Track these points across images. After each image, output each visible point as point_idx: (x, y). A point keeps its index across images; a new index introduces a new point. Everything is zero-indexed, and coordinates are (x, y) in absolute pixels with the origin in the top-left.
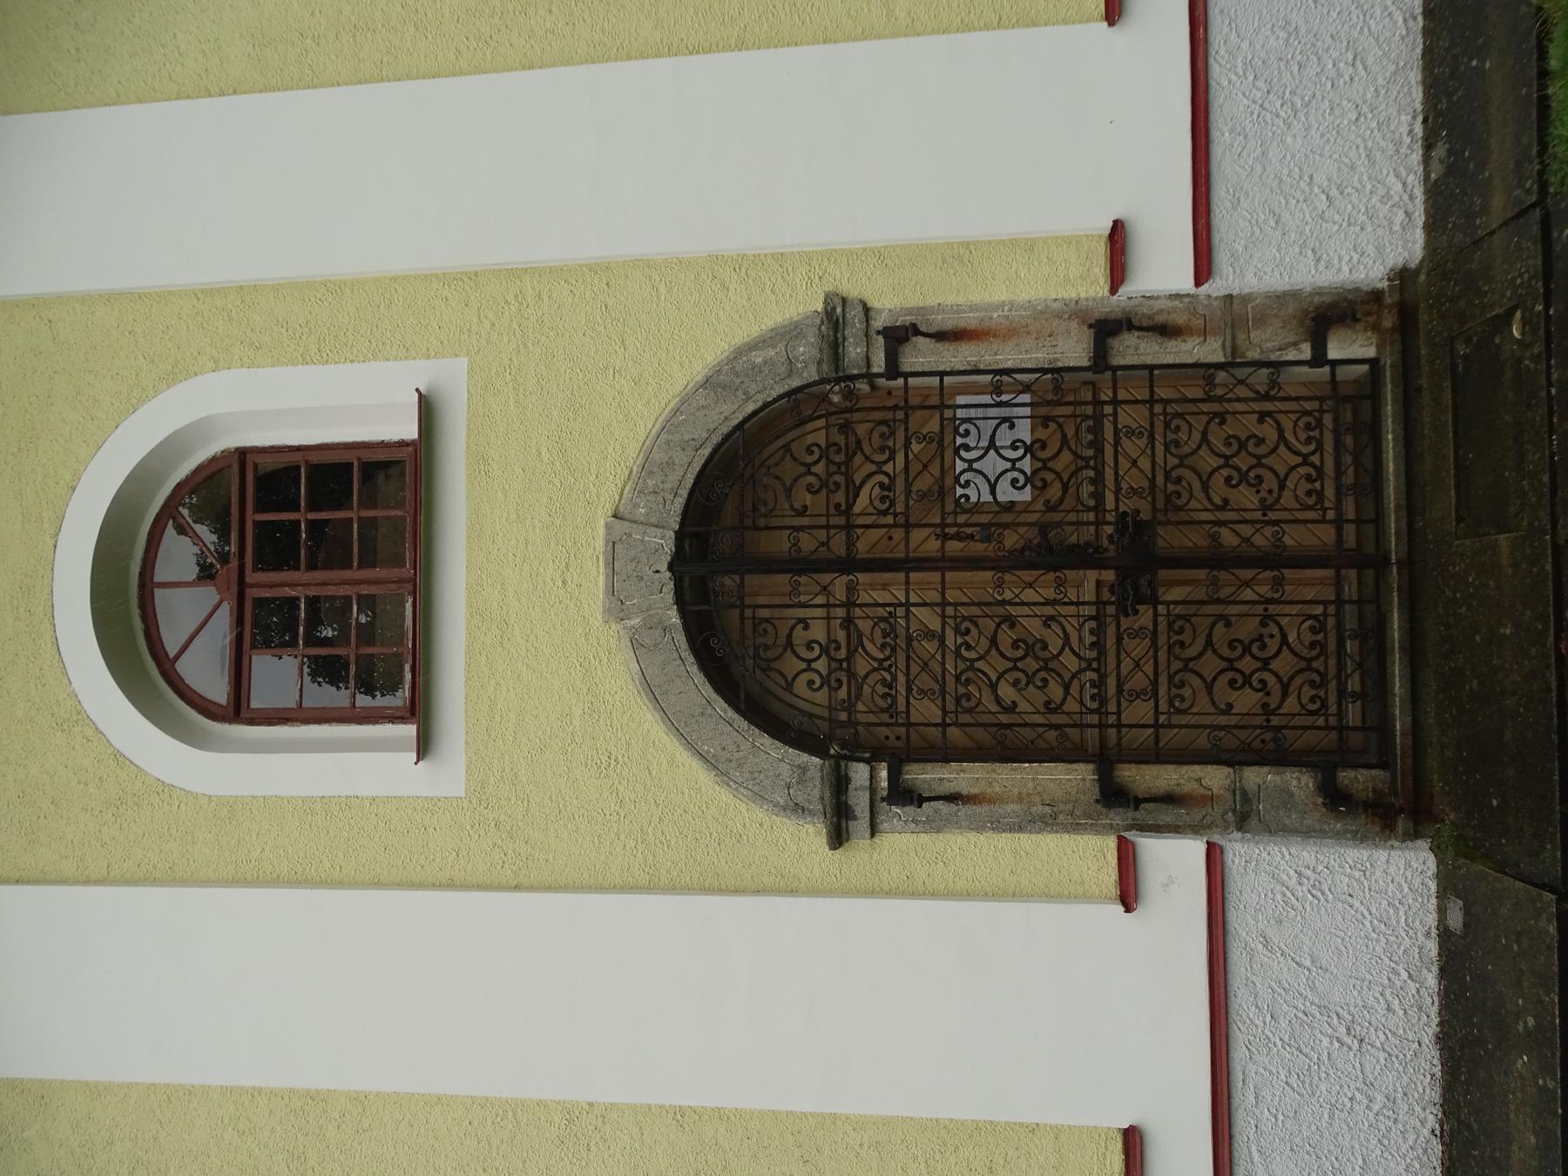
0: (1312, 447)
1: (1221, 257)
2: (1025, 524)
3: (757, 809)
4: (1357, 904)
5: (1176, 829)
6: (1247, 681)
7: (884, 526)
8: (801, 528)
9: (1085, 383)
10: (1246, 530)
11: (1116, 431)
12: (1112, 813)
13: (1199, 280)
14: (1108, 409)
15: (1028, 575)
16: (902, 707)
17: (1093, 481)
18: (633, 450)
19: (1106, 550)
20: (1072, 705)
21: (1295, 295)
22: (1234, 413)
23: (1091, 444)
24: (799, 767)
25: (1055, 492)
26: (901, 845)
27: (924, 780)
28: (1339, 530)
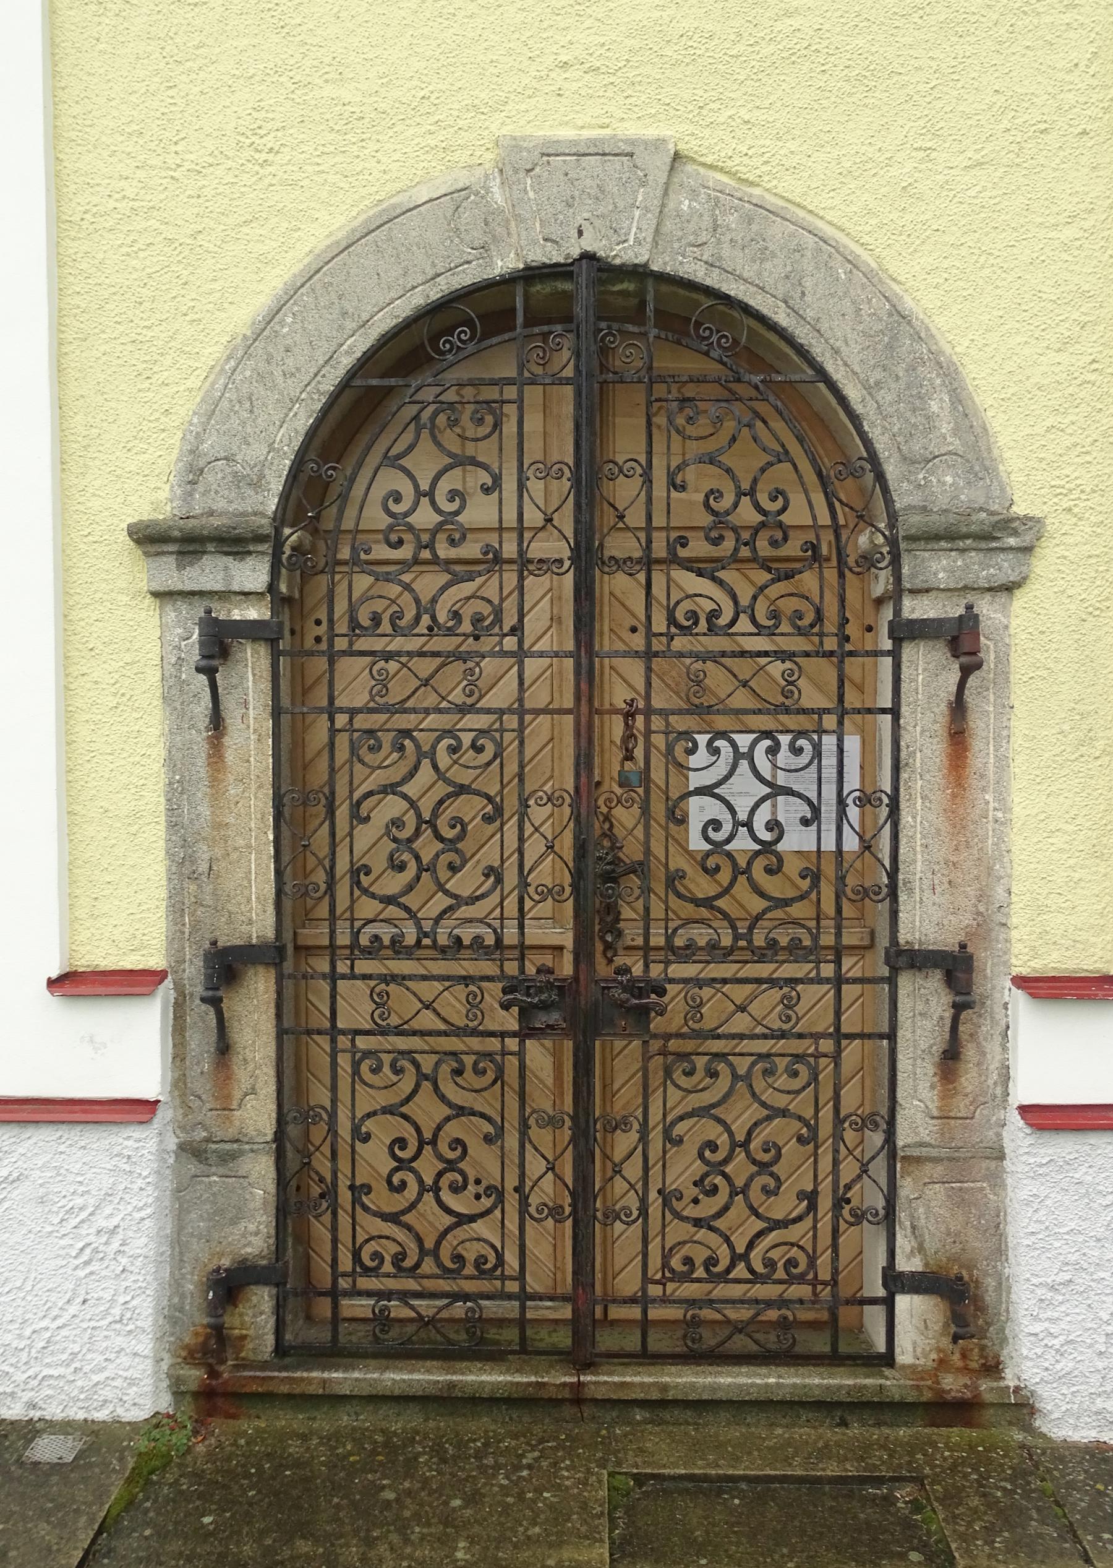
0: (759, 1268)
1: (1065, 1146)
2: (647, 835)
3: (192, 406)
4: (73, 1309)
5: (179, 1055)
6: (402, 1165)
7: (649, 618)
8: (648, 480)
9: (872, 934)
10: (632, 1169)
11: (793, 982)
12: (200, 963)
13: (1024, 1110)
14: (828, 970)
15: (566, 844)
16: (362, 644)
17: (713, 946)
18: (790, 187)
19: (610, 961)
20: (368, 908)
21: (1000, 1251)
22: (816, 1154)
23: (773, 944)
24: (262, 476)
25: (703, 887)
26: (141, 639)
27: (243, 678)
28: (633, 1300)
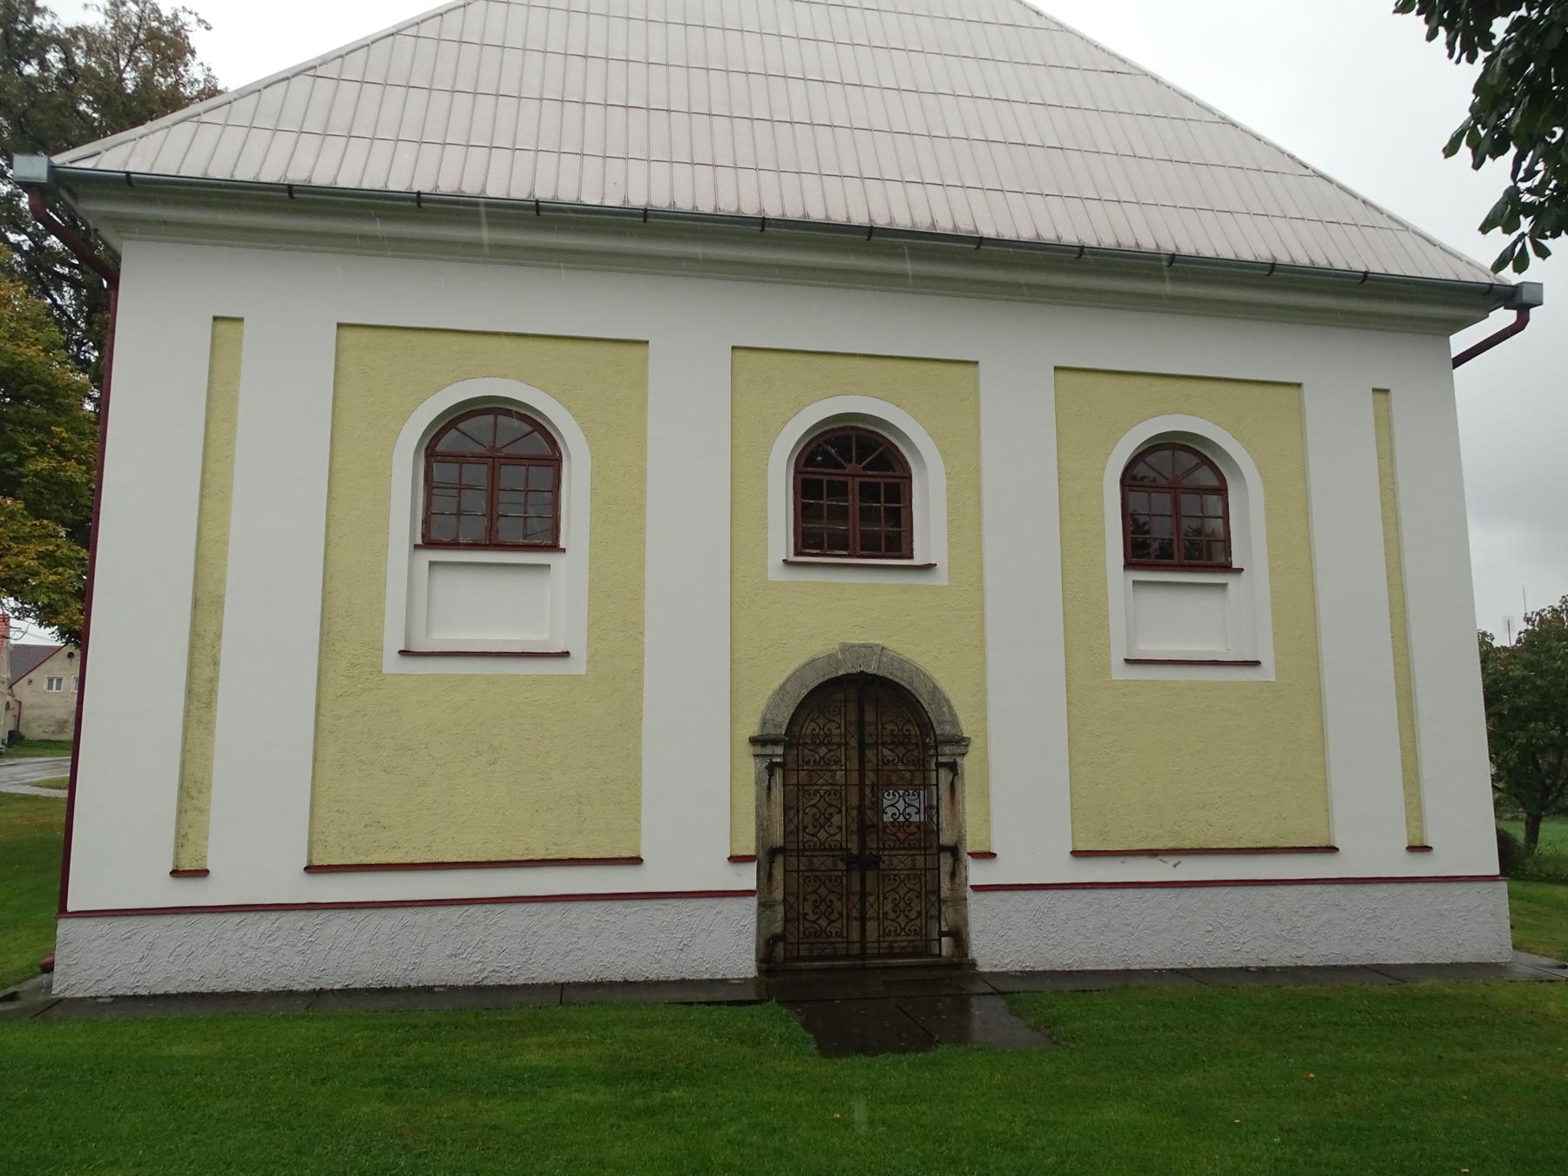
1: (981, 895)
21: (966, 924)
26: (750, 767)
